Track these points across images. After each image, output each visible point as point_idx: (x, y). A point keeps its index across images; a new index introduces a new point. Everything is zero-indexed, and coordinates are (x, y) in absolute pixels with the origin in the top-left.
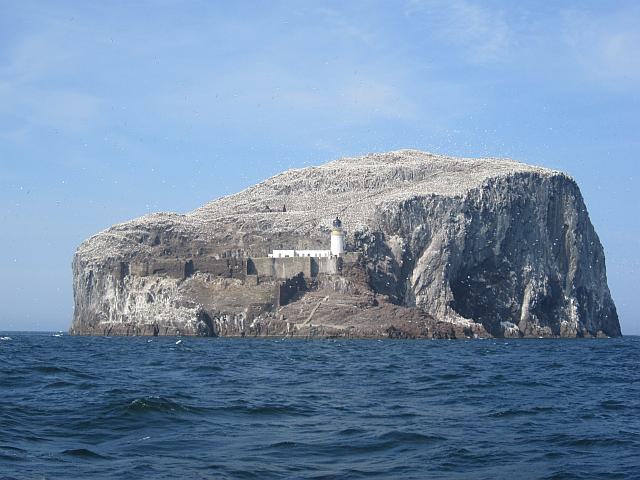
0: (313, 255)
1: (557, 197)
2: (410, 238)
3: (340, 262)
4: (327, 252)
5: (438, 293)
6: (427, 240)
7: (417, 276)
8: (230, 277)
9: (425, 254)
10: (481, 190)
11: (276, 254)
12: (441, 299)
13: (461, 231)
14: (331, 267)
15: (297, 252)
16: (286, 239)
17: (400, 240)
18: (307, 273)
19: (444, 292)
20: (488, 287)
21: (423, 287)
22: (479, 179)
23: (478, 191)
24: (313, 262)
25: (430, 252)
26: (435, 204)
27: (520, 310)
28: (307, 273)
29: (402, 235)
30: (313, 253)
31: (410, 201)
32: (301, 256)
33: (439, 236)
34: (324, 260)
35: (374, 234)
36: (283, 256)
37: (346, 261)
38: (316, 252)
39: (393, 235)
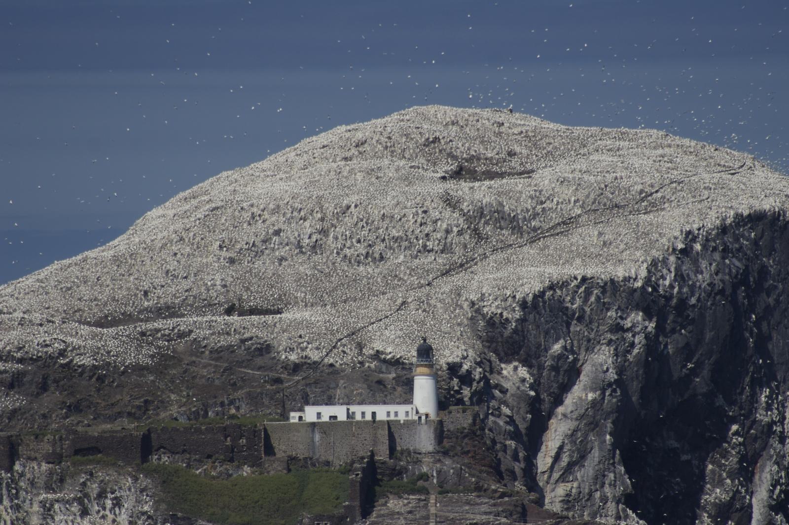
0: (381, 416)
1: (748, 497)
2: (541, 367)
3: (440, 433)
4: (407, 408)
5: (599, 478)
6: (574, 372)
7: (558, 444)
8: (231, 460)
9: (570, 400)
10: (672, 259)
11: (310, 414)
12: (607, 489)
13: (636, 351)
14: (425, 441)
15: (353, 408)
16: (319, 381)
17: (523, 372)
18: (382, 455)
19: (612, 476)
20: (685, 457)
21: (571, 466)
22: (672, 224)
23: (665, 261)
24: (390, 426)
25: (580, 394)
26: (588, 293)
27: (750, 506)
28: (382, 455)
29: (526, 363)
30: (382, 412)
31: (542, 294)
32: (358, 417)
33: (600, 360)
34: (409, 424)
35: (479, 364)
36: (325, 418)
37: (449, 426)
38: (392, 408)
39: (508, 362)
